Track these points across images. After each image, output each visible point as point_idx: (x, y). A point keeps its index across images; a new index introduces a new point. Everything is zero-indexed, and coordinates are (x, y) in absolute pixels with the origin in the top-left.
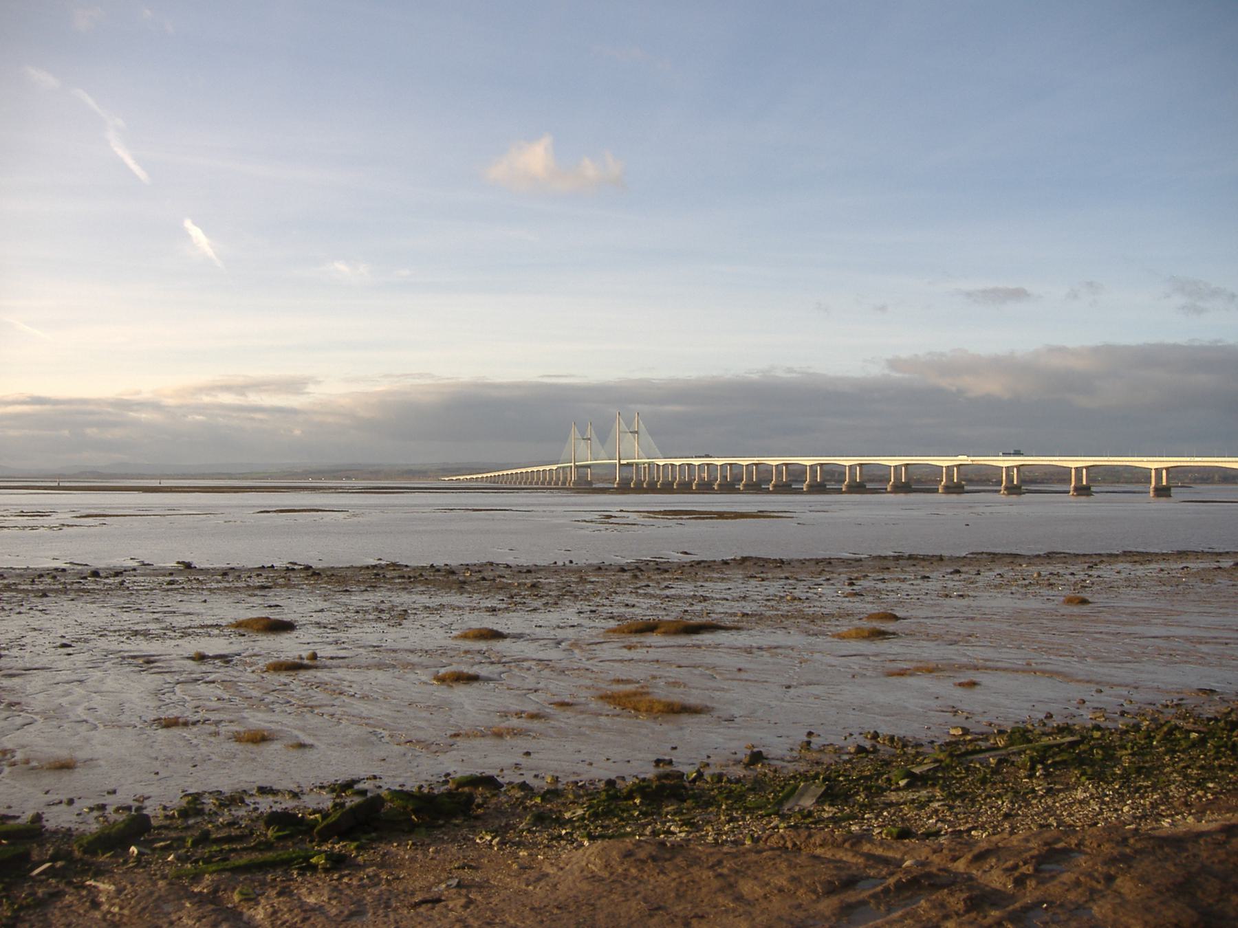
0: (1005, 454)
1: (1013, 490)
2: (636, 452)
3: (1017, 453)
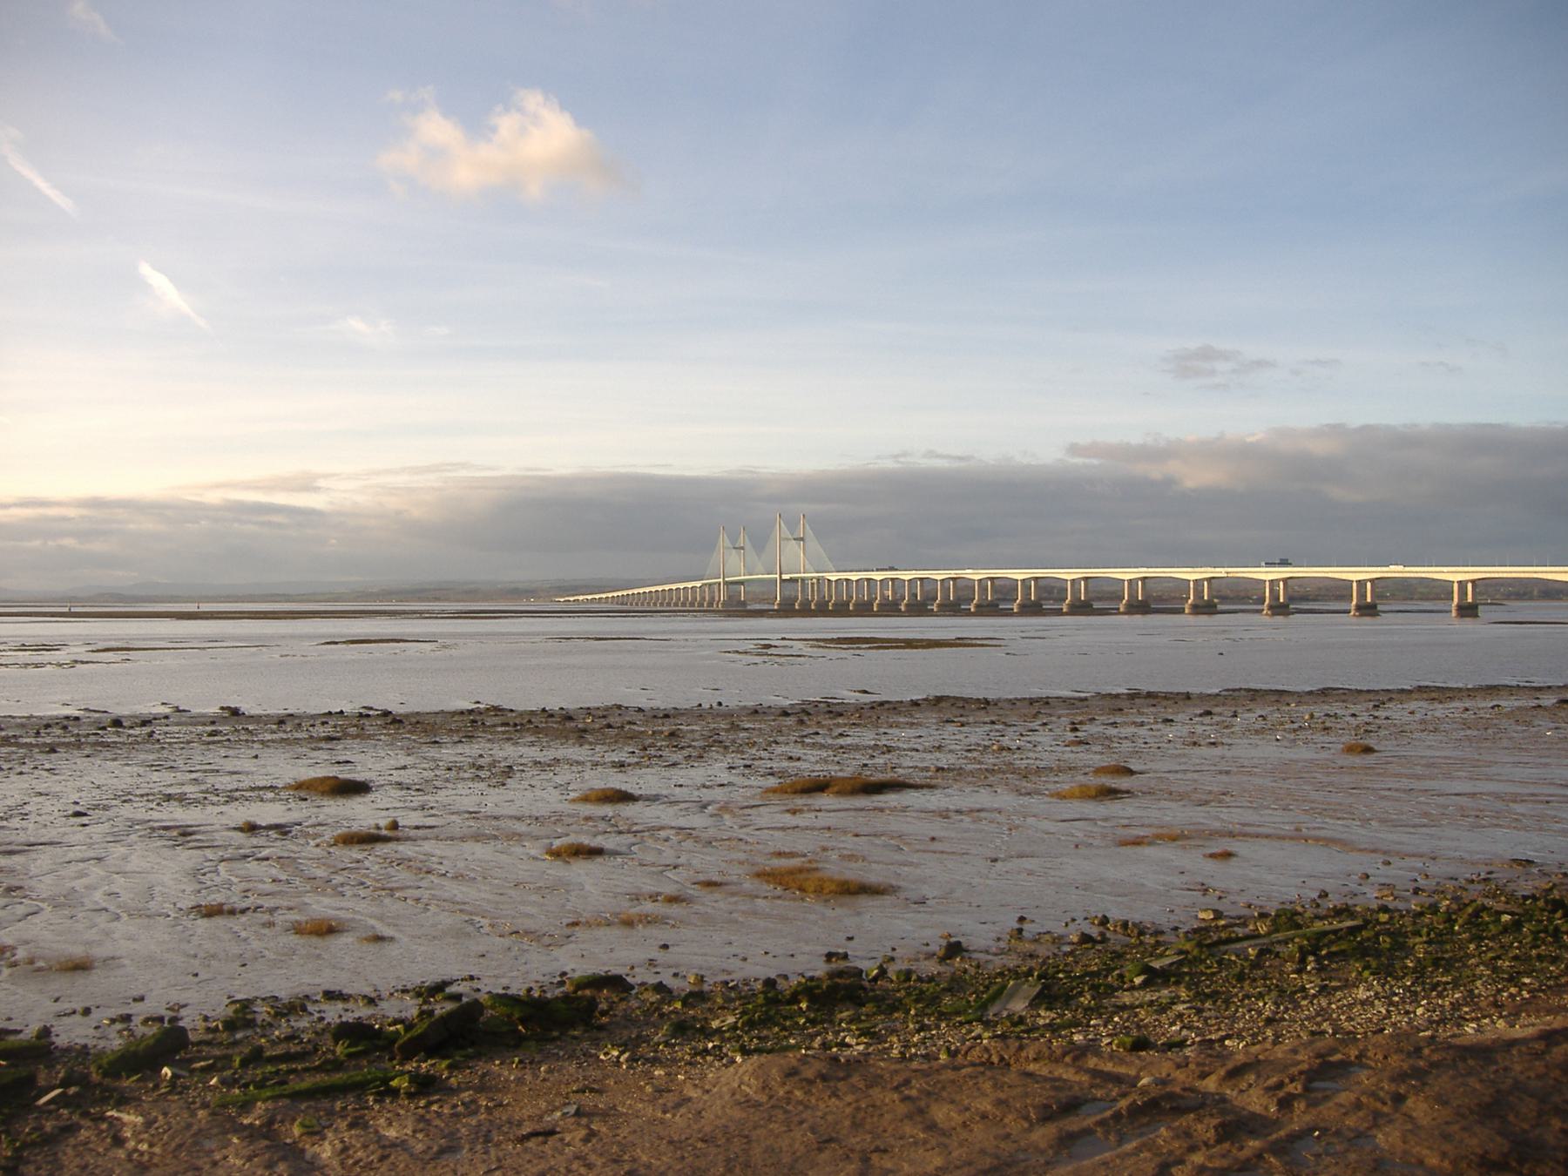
0: (1268, 564)
1: (1279, 609)
2: (801, 562)
3: (1284, 563)
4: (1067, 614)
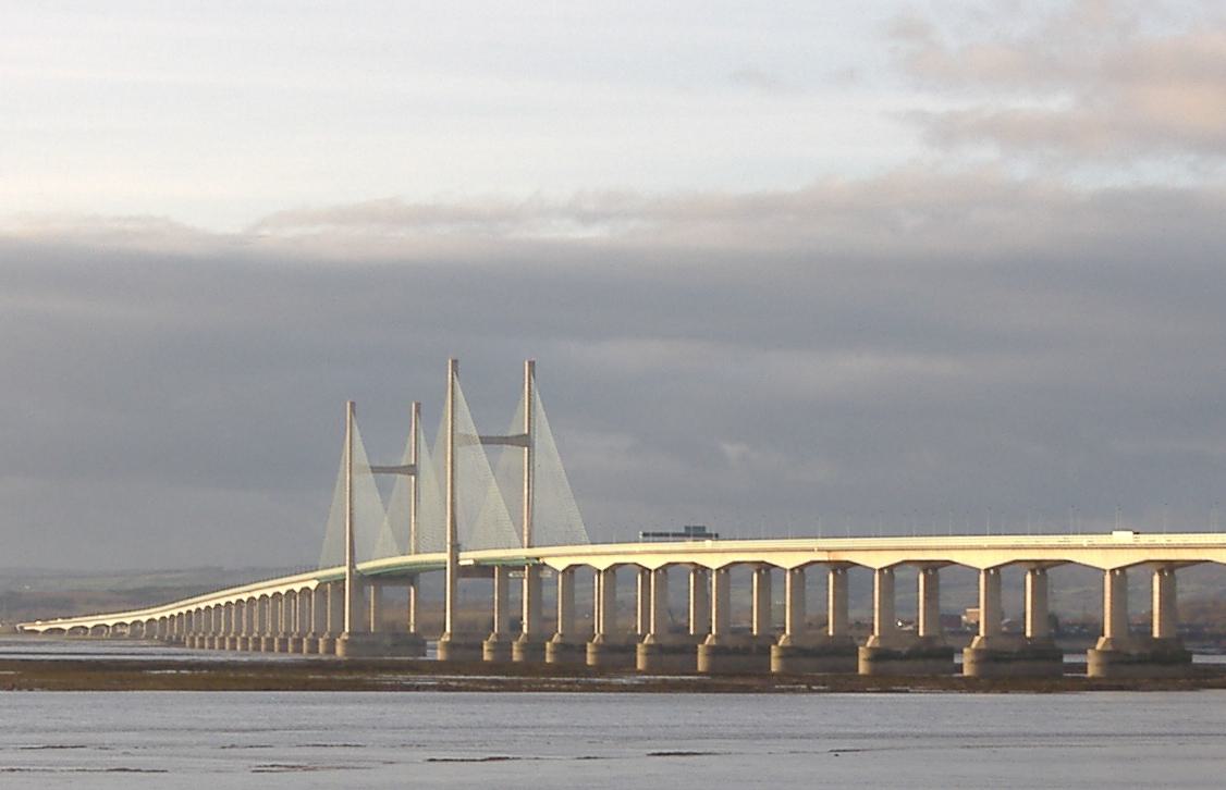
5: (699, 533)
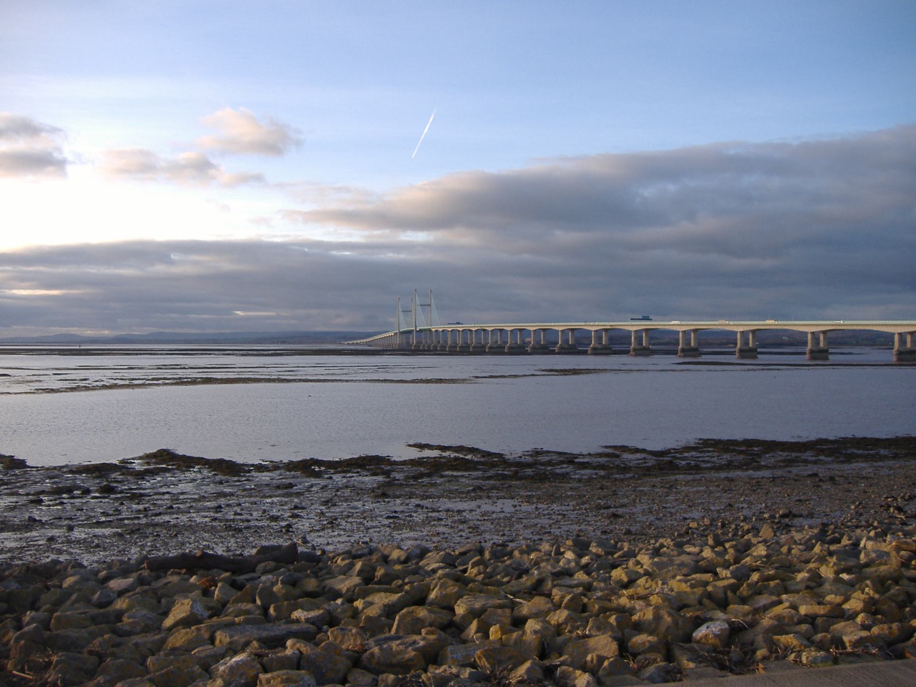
4: (559, 353)
5: (458, 323)
